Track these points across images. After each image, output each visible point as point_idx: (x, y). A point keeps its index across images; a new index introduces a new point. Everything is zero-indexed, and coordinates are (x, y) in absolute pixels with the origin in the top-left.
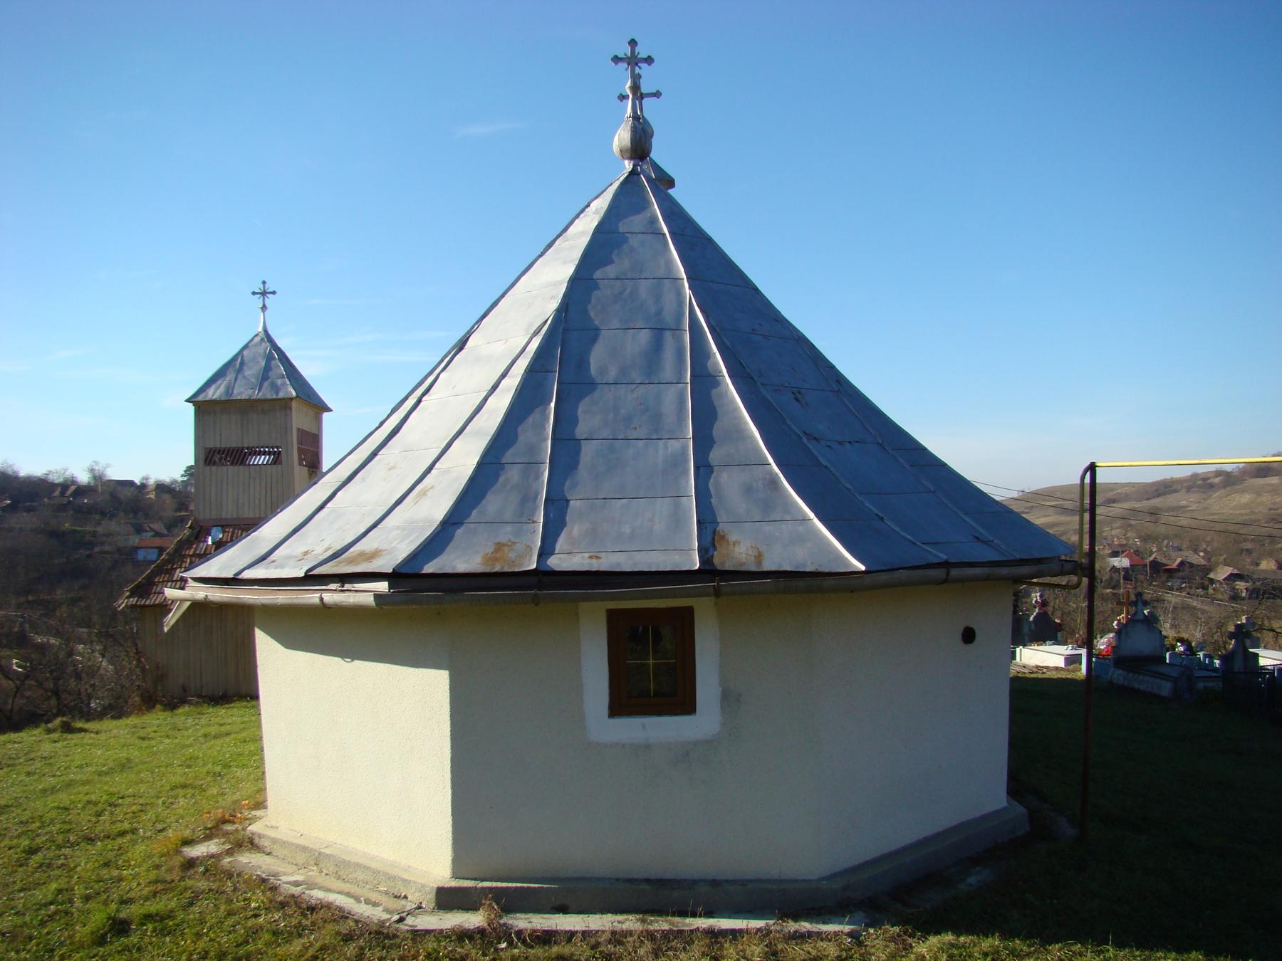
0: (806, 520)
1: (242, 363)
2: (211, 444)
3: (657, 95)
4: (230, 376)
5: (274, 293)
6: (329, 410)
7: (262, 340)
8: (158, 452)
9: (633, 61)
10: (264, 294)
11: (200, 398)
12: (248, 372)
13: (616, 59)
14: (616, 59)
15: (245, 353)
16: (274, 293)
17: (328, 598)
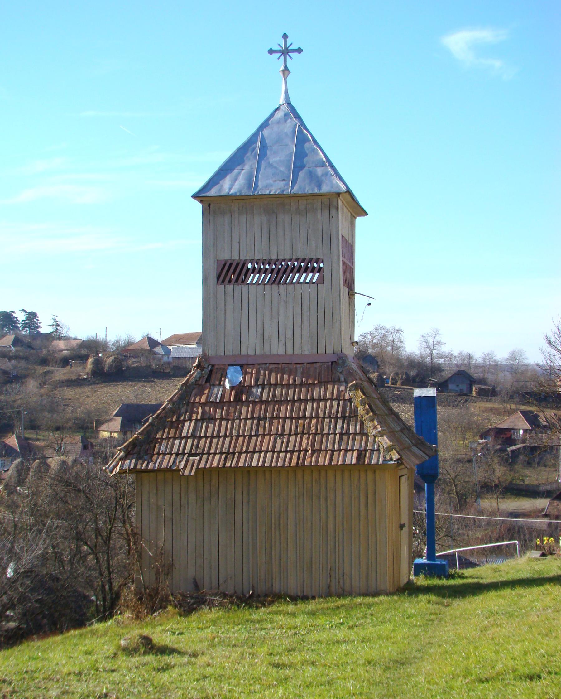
1: (264, 146)
2: (226, 256)
4: (250, 165)
5: (299, 51)
7: (286, 115)
10: (285, 52)
11: (213, 192)
12: (273, 159)
15: (266, 132)
16: (299, 51)
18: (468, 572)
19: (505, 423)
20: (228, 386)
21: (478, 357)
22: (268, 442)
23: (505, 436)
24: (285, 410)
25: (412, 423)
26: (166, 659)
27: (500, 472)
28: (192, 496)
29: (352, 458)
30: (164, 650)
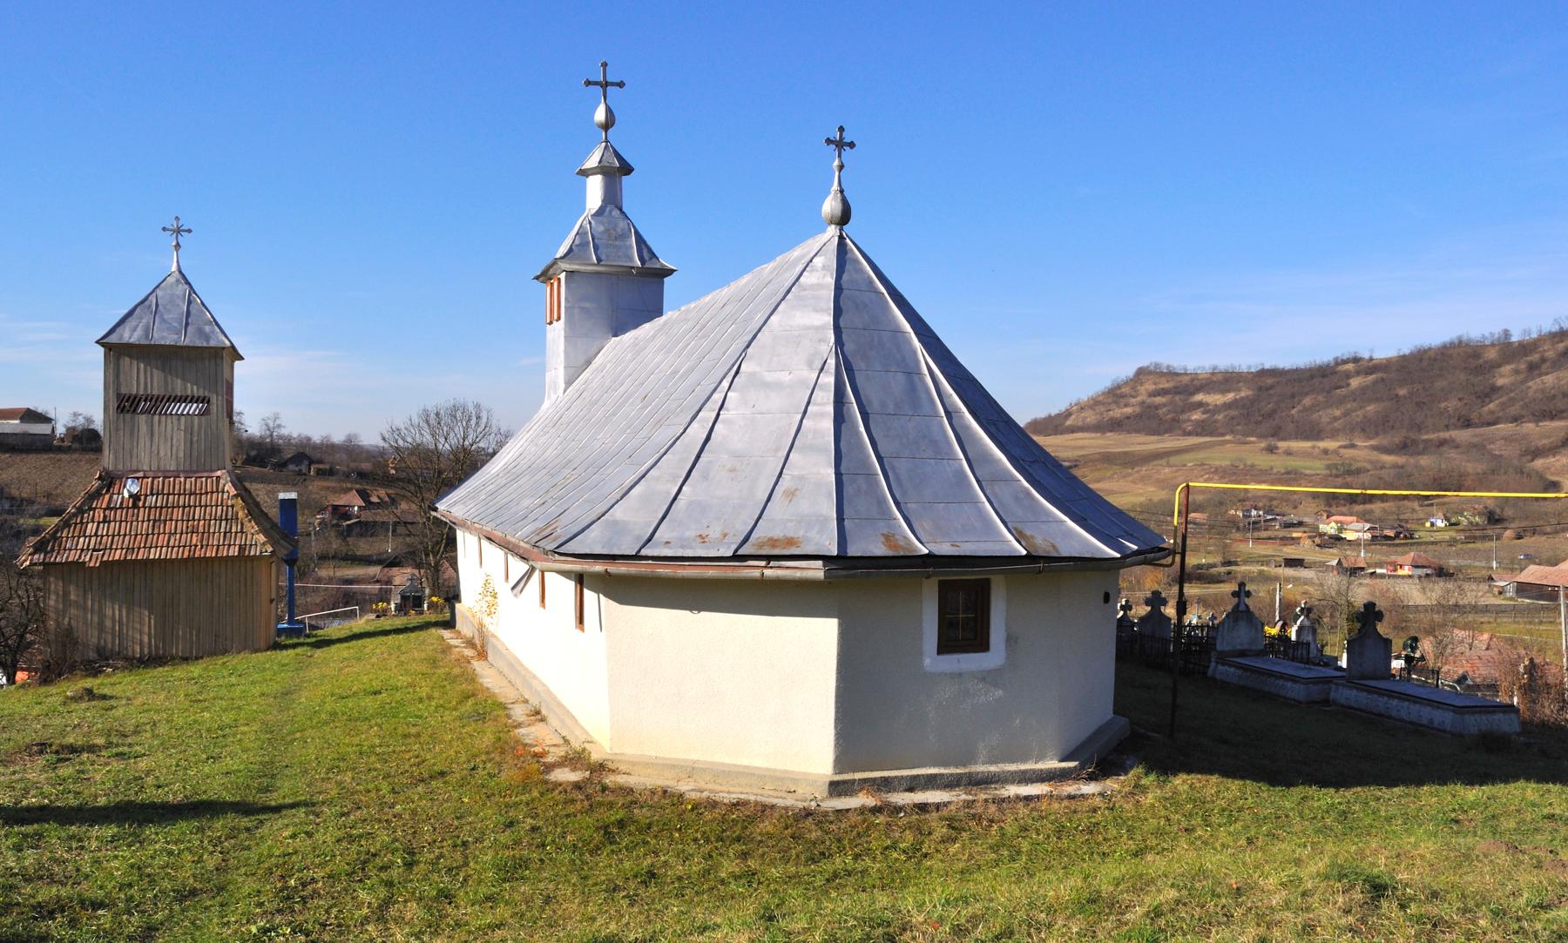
0: (1063, 522)
3: (621, 85)
6: (242, 358)
8: (76, 395)
9: (840, 145)
10: (178, 231)
11: (113, 339)
13: (829, 141)
14: (829, 141)
15: (159, 292)
17: (768, 573)
18: (320, 632)
19: (342, 500)
20: (126, 495)
21: (317, 438)
22: (163, 540)
23: (341, 512)
24: (178, 514)
25: (277, 520)
26: (108, 703)
27: (336, 545)
28: (95, 583)
29: (234, 551)
30: (104, 697)
